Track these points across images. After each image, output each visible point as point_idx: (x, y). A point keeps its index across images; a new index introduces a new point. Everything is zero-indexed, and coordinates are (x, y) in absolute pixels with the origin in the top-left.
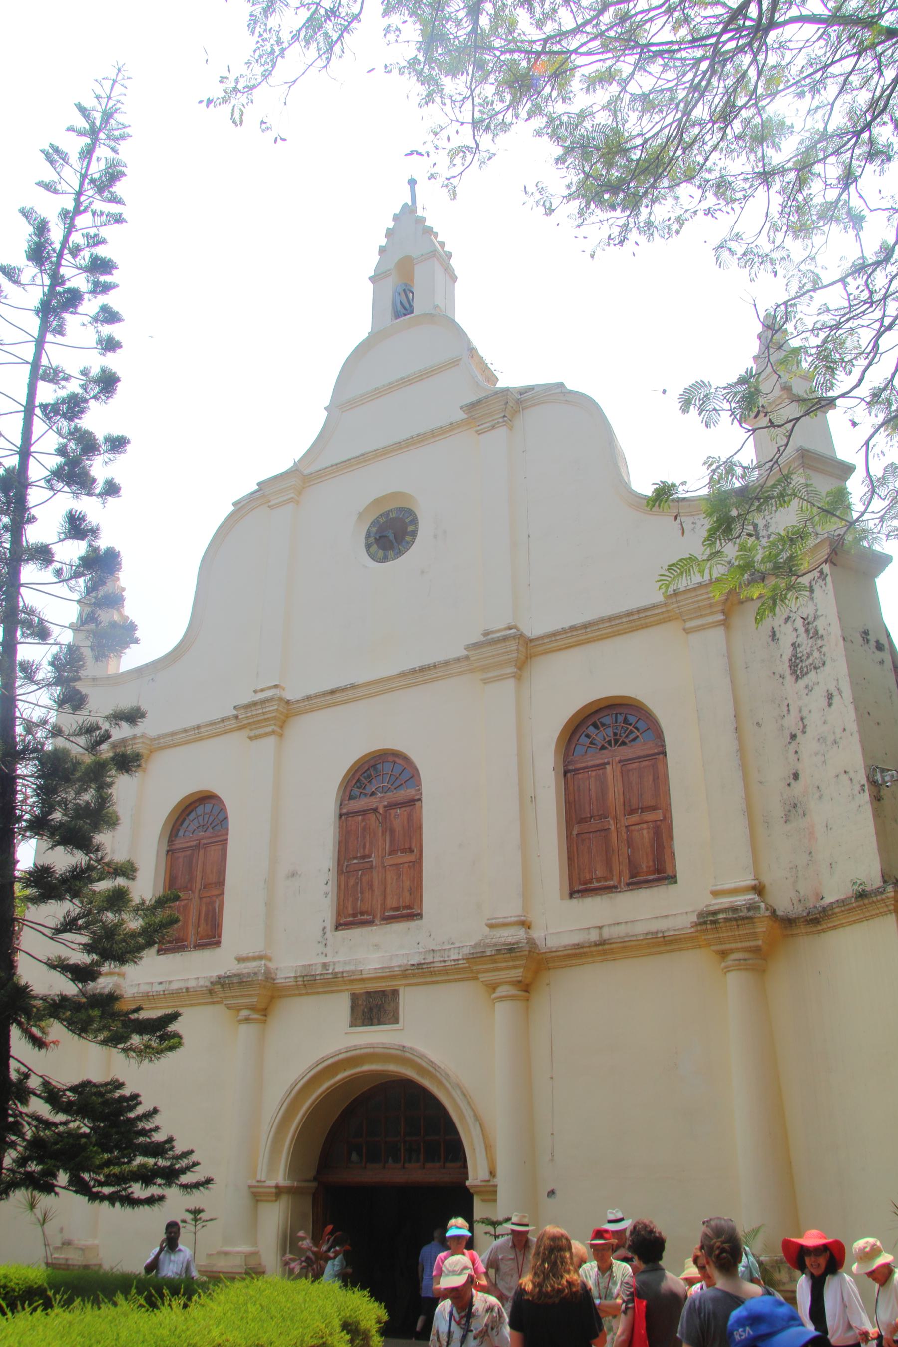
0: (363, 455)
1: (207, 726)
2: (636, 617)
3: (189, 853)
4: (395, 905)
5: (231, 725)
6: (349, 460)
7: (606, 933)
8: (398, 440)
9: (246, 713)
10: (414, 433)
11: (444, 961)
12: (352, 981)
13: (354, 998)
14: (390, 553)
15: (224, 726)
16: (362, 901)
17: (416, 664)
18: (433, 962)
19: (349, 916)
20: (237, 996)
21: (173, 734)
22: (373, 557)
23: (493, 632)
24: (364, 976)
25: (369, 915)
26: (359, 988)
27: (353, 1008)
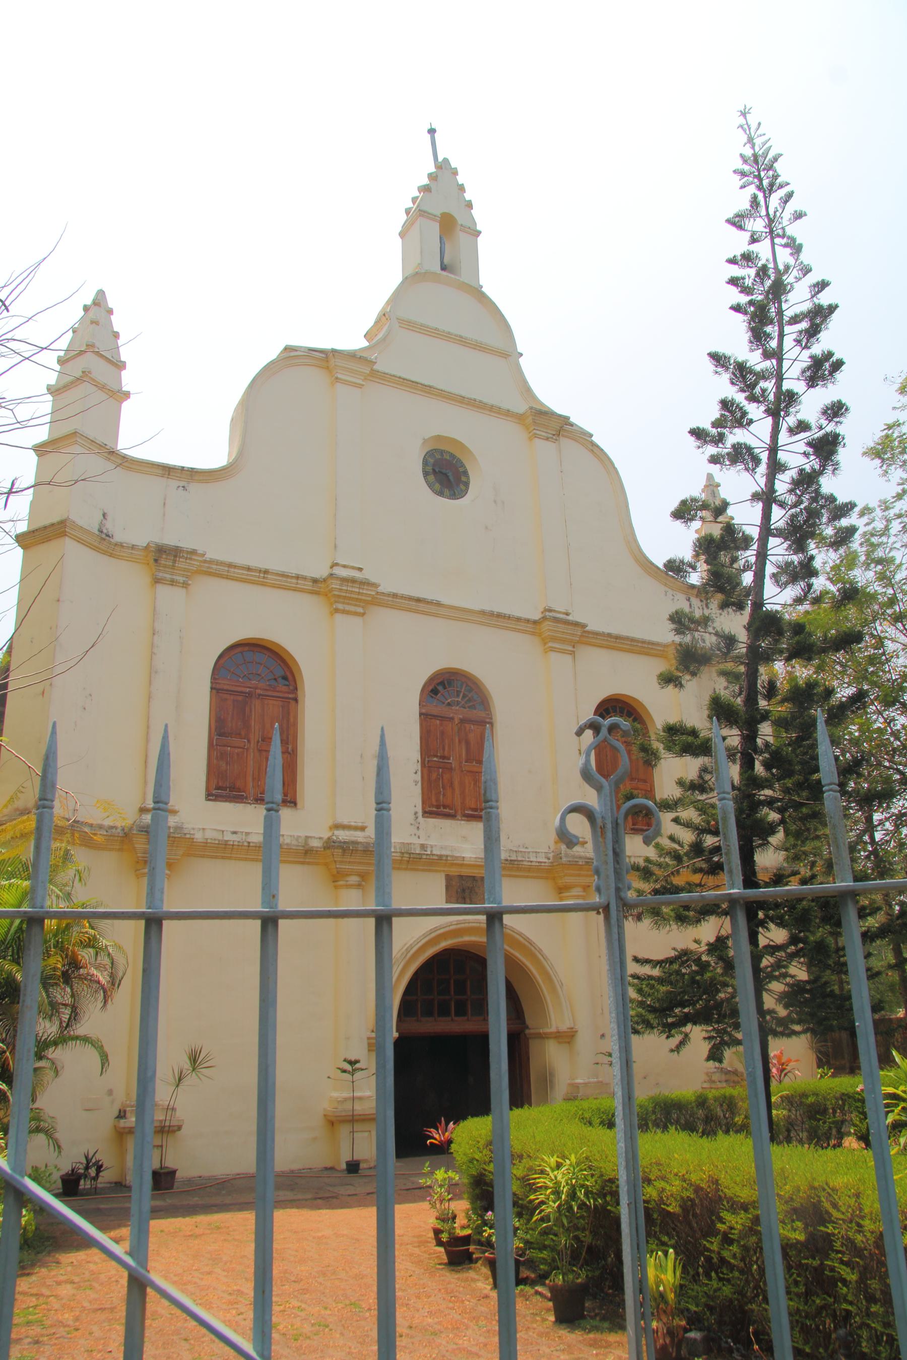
0: (430, 387)
1: (277, 574)
2: (640, 645)
3: (240, 698)
4: (473, 806)
5: (304, 585)
6: (417, 383)
7: (228, 837)
8: (463, 395)
9: (341, 585)
10: (478, 398)
11: (531, 862)
12: (452, 865)
13: (449, 878)
14: (447, 492)
15: (297, 583)
16: (444, 795)
17: (496, 610)
18: (522, 861)
19: (433, 806)
20: (354, 862)
21: (230, 565)
22: (430, 486)
23: (555, 611)
24: (465, 862)
25: (451, 809)
26: (454, 871)
27: (448, 887)
